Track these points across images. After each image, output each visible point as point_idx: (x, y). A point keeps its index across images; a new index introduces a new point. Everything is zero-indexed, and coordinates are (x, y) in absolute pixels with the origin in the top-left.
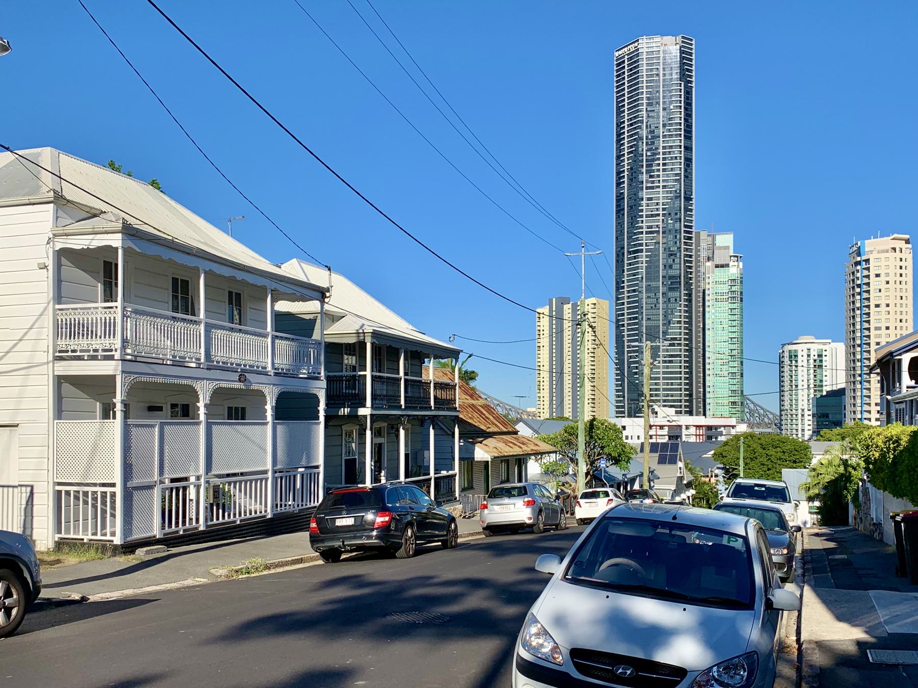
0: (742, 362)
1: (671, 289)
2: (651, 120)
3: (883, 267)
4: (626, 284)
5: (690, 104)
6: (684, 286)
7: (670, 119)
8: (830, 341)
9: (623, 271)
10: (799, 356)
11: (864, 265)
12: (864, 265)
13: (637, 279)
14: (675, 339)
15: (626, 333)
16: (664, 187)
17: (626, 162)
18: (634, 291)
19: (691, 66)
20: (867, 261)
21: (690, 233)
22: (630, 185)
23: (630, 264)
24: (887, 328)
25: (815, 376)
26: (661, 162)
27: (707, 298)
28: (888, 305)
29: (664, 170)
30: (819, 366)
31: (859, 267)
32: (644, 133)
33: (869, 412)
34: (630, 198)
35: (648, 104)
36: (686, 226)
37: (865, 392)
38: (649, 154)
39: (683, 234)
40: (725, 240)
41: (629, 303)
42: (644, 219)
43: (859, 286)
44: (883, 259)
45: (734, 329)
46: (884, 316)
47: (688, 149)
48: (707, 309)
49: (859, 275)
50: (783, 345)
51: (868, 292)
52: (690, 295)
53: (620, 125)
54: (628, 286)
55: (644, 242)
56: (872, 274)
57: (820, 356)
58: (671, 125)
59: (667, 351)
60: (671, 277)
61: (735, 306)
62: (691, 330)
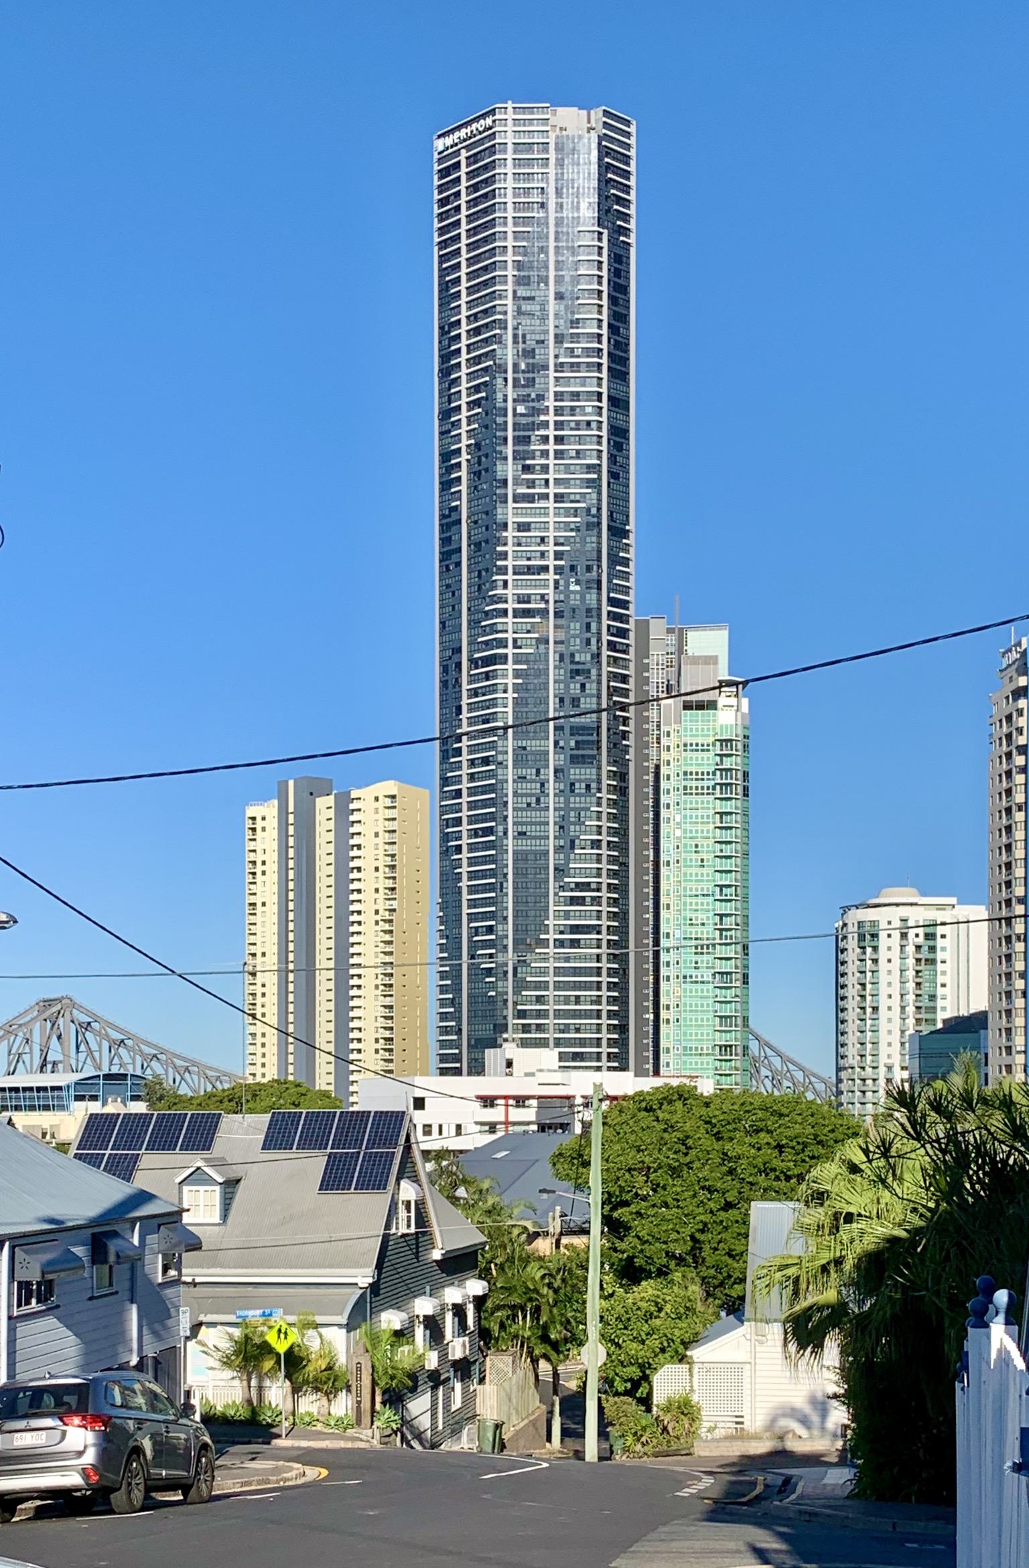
1: (575, 760)
2: (525, 321)
6: (607, 743)
7: (575, 323)
8: (953, 900)
9: (459, 710)
14: (585, 886)
16: (559, 498)
18: (486, 761)
22: (473, 488)
23: (475, 693)
25: (918, 984)
26: (551, 432)
27: (664, 785)
30: (927, 959)
32: (508, 354)
35: (521, 281)
36: (612, 602)
38: (521, 409)
39: (605, 622)
40: (710, 643)
42: (510, 577)
47: (618, 403)
50: (845, 909)
52: (622, 776)
53: (448, 329)
55: (510, 636)
58: (575, 337)
59: (567, 915)
60: (575, 731)
61: (728, 807)
62: (625, 865)
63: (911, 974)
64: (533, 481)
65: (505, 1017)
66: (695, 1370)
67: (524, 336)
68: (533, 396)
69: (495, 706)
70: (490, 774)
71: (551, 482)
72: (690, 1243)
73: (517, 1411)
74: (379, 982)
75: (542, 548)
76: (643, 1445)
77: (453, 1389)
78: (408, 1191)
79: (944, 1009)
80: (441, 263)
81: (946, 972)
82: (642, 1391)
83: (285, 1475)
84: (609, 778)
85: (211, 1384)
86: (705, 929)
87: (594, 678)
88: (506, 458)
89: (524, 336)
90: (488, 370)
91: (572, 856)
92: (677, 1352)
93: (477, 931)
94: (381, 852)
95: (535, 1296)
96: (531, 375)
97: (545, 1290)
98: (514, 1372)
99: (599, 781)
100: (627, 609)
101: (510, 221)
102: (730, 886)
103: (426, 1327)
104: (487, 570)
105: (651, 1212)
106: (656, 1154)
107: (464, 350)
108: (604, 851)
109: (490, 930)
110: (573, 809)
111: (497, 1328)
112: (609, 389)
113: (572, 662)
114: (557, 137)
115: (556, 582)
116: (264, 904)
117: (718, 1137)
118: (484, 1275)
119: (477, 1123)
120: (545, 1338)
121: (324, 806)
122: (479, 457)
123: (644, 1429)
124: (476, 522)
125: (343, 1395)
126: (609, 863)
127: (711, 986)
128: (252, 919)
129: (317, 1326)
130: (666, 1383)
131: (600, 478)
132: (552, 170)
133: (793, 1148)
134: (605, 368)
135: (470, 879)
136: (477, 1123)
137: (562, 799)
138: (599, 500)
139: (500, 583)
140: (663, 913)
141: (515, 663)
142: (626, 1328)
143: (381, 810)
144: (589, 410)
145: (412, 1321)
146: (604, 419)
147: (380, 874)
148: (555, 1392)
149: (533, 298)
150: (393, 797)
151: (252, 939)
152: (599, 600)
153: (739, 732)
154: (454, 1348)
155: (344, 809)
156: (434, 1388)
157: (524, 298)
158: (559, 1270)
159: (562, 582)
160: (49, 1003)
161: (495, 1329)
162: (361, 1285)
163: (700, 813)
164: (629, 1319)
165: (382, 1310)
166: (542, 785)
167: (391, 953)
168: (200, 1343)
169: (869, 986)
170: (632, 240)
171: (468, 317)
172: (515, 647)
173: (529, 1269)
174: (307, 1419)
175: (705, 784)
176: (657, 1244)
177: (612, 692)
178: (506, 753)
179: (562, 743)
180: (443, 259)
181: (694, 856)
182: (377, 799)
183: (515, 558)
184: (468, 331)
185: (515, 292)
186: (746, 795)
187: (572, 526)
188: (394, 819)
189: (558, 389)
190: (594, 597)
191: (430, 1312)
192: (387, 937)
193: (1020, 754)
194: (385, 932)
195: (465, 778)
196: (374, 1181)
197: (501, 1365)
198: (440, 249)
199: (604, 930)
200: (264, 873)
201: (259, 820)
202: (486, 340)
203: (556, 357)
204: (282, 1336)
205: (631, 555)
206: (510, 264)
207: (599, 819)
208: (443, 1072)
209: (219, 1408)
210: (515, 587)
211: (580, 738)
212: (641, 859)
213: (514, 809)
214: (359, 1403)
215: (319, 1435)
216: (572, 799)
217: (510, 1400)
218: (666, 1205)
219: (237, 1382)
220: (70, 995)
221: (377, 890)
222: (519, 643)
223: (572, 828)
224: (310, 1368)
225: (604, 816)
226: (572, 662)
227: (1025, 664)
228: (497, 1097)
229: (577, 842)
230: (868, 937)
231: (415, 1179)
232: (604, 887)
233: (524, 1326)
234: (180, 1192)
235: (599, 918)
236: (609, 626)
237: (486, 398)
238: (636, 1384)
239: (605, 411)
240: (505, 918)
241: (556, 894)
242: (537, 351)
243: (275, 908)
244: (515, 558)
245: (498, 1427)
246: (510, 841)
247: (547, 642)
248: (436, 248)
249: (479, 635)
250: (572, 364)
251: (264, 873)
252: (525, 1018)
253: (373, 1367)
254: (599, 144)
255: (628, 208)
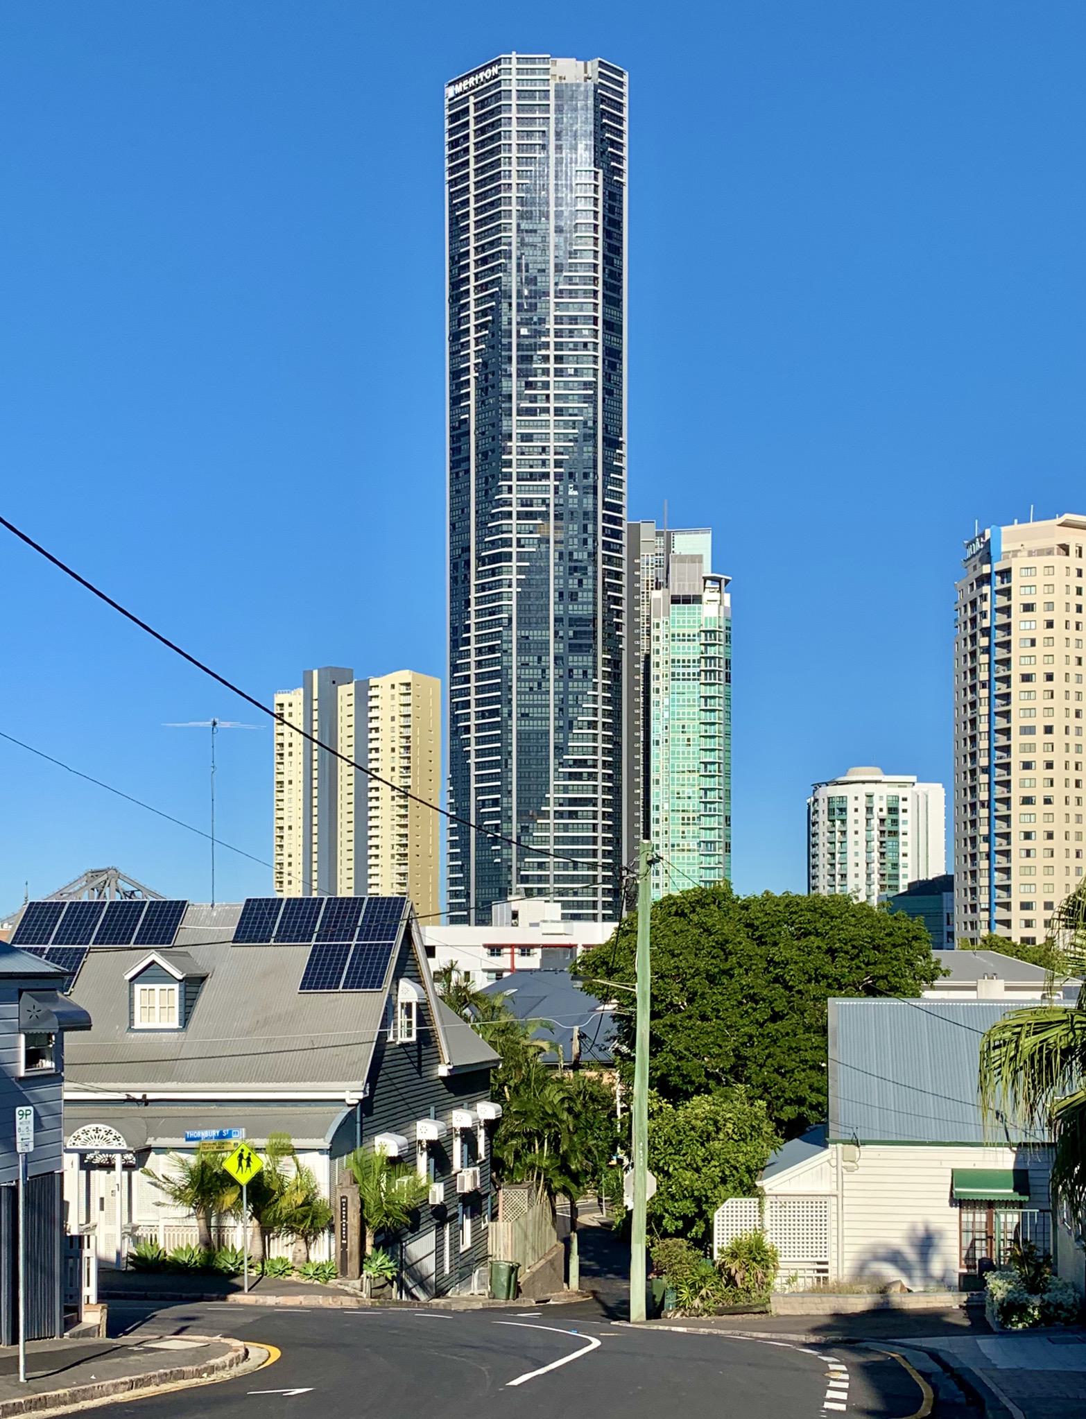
0: (728, 819)
1: (575, 648)
2: (527, 251)
3: (1040, 588)
4: (473, 633)
5: (617, 224)
6: (603, 639)
7: (573, 254)
8: (913, 779)
9: (468, 603)
10: (850, 810)
11: (998, 583)
12: (998, 583)
13: (498, 623)
14: (583, 763)
15: (473, 747)
16: (559, 412)
17: (473, 348)
18: (492, 649)
19: (620, 133)
20: (1006, 574)
21: (617, 521)
22: (481, 402)
23: (482, 588)
24: (1049, 730)
25: (882, 854)
26: (552, 353)
27: (654, 671)
28: (1050, 677)
29: (559, 373)
30: (890, 831)
31: (986, 589)
32: (513, 281)
33: (1007, 923)
34: (481, 434)
35: (522, 216)
36: (607, 506)
37: (998, 878)
38: (524, 331)
39: (601, 524)
40: (695, 544)
41: (479, 677)
42: (514, 483)
43: (986, 632)
44: (1040, 570)
45: (710, 744)
46: (1040, 703)
47: (612, 327)
48: (654, 697)
49: (986, 606)
50: (817, 786)
51: (1007, 645)
52: (615, 663)
53: (457, 259)
54: (479, 639)
55: (514, 536)
56: (1016, 603)
57: (893, 810)
59: (566, 789)
60: (574, 621)
61: (711, 691)
62: (618, 744)
63: (876, 844)
64: (535, 396)
65: (510, 882)
66: (767, 1205)
67: (527, 265)
68: (535, 319)
69: (501, 599)
70: (497, 661)
71: (552, 398)
72: (733, 1059)
73: (533, 1248)
74: (395, 852)
75: (544, 457)
76: (703, 1299)
77: (462, 1227)
78: (408, 992)
79: (905, 876)
80: (451, 200)
81: (907, 843)
82: (698, 1230)
83: (213, 1362)
84: (604, 665)
85: (162, 1223)
86: (691, 802)
87: (590, 574)
88: (510, 376)
89: (527, 265)
90: (495, 295)
91: (570, 736)
92: (741, 1183)
93: (483, 804)
94: (397, 735)
95: (554, 1121)
96: (533, 301)
97: (565, 1116)
98: (530, 1206)
99: (595, 668)
100: (620, 512)
101: (514, 161)
102: (714, 763)
103: (430, 1155)
104: (493, 476)
105: (687, 1023)
106: (691, 958)
107: (472, 278)
108: (600, 731)
109: (495, 802)
110: (571, 693)
111: (511, 1158)
112: (604, 313)
113: (571, 560)
114: (557, 85)
115: (556, 488)
116: (290, 782)
117: (760, 941)
118: (497, 1098)
119: (484, 970)
120: (564, 1169)
121: (345, 693)
122: (486, 375)
123: (703, 1279)
124: (483, 433)
125: (324, 1238)
126: (604, 741)
127: (697, 854)
128: (280, 796)
129: (293, 1151)
130: (731, 1221)
131: (596, 394)
132: (552, 115)
133: (847, 953)
134: (600, 295)
135: (477, 757)
136: (484, 970)
137: (561, 684)
138: (595, 414)
139: (505, 489)
140: (653, 788)
141: (518, 561)
142: (677, 1153)
143: (397, 696)
144: (586, 332)
145: (413, 1147)
146: (600, 341)
147: (396, 754)
148: (573, 1228)
149: (535, 231)
150: (408, 685)
151: (280, 814)
152: (595, 505)
153: (722, 624)
154: (463, 1179)
155: (363, 698)
156: (440, 1227)
157: (527, 231)
158: (580, 1093)
159: (561, 488)
160: (96, 873)
161: (509, 1159)
162: (349, 1102)
163: (686, 697)
164: (680, 1142)
165: (376, 1133)
166: (544, 671)
167: (406, 826)
168: (148, 1173)
169: (838, 856)
170: (625, 180)
171: (476, 248)
172: (519, 546)
173: (546, 1092)
174: (279, 1267)
175: (691, 670)
176: (695, 1060)
177: (607, 587)
178: (511, 642)
179: (561, 633)
180: (453, 195)
181: (681, 736)
182: (393, 686)
183: (519, 466)
184: (476, 261)
185: (518, 225)
186: (728, 680)
187: (571, 437)
188: (409, 705)
189: (558, 313)
190: (591, 501)
191: (434, 1137)
192: (403, 812)
193: (983, 636)
194: (400, 806)
195: (473, 665)
196: (367, 976)
197: (516, 1200)
198: (450, 187)
199: (600, 802)
200: (290, 754)
201: (286, 706)
202: (492, 269)
203: (556, 284)
204: (244, 1163)
205: (624, 464)
206: (514, 200)
207: (595, 702)
208: (454, 920)
209: (169, 1254)
210: (519, 492)
211: (578, 629)
212: (632, 740)
213: (518, 693)
214: (344, 1246)
215: (294, 1289)
216: (570, 684)
217: (526, 1237)
218: (704, 1018)
219: (193, 1221)
220: (116, 866)
221: (393, 769)
222: (522, 542)
223: (571, 710)
224: (283, 1203)
225: (600, 700)
226: (571, 560)
227: (989, 553)
228: (503, 946)
229: (575, 723)
230: (837, 811)
231: (417, 978)
232: (600, 764)
233: (542, 1155)
234: (131, 991)
235: (595, 792)
236: (604, 528)
237: (493, 321)
238: (689, 1222)
239: (600, 334)
240: (510, 792)
241: (556, 770)
242: (539, 279)
243: (301, 786)
244: (519, 466)
245: (513, 1270)
246: (514, 723)
247: (548, 541)
248: (447, 186)
249: (486, 536)
250: (570, 291)
251: (290, 754)
252: (527, 882)
253: (362, 1202)
254: (595, 91)
255: (622, 150)
